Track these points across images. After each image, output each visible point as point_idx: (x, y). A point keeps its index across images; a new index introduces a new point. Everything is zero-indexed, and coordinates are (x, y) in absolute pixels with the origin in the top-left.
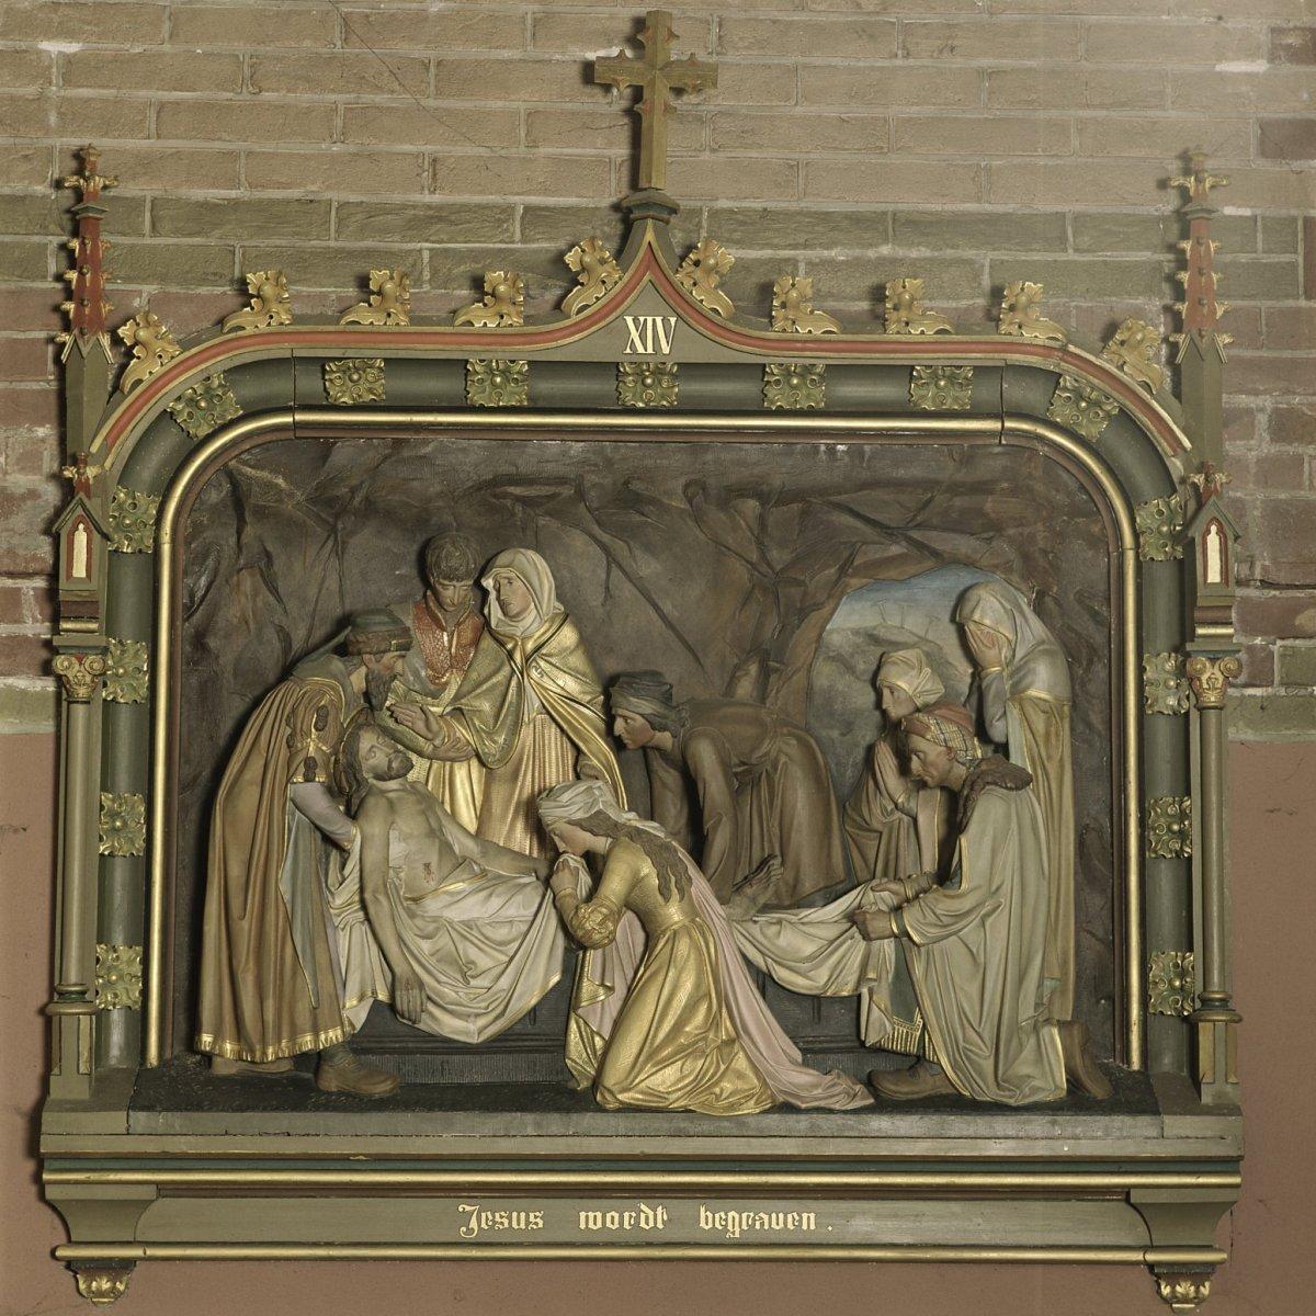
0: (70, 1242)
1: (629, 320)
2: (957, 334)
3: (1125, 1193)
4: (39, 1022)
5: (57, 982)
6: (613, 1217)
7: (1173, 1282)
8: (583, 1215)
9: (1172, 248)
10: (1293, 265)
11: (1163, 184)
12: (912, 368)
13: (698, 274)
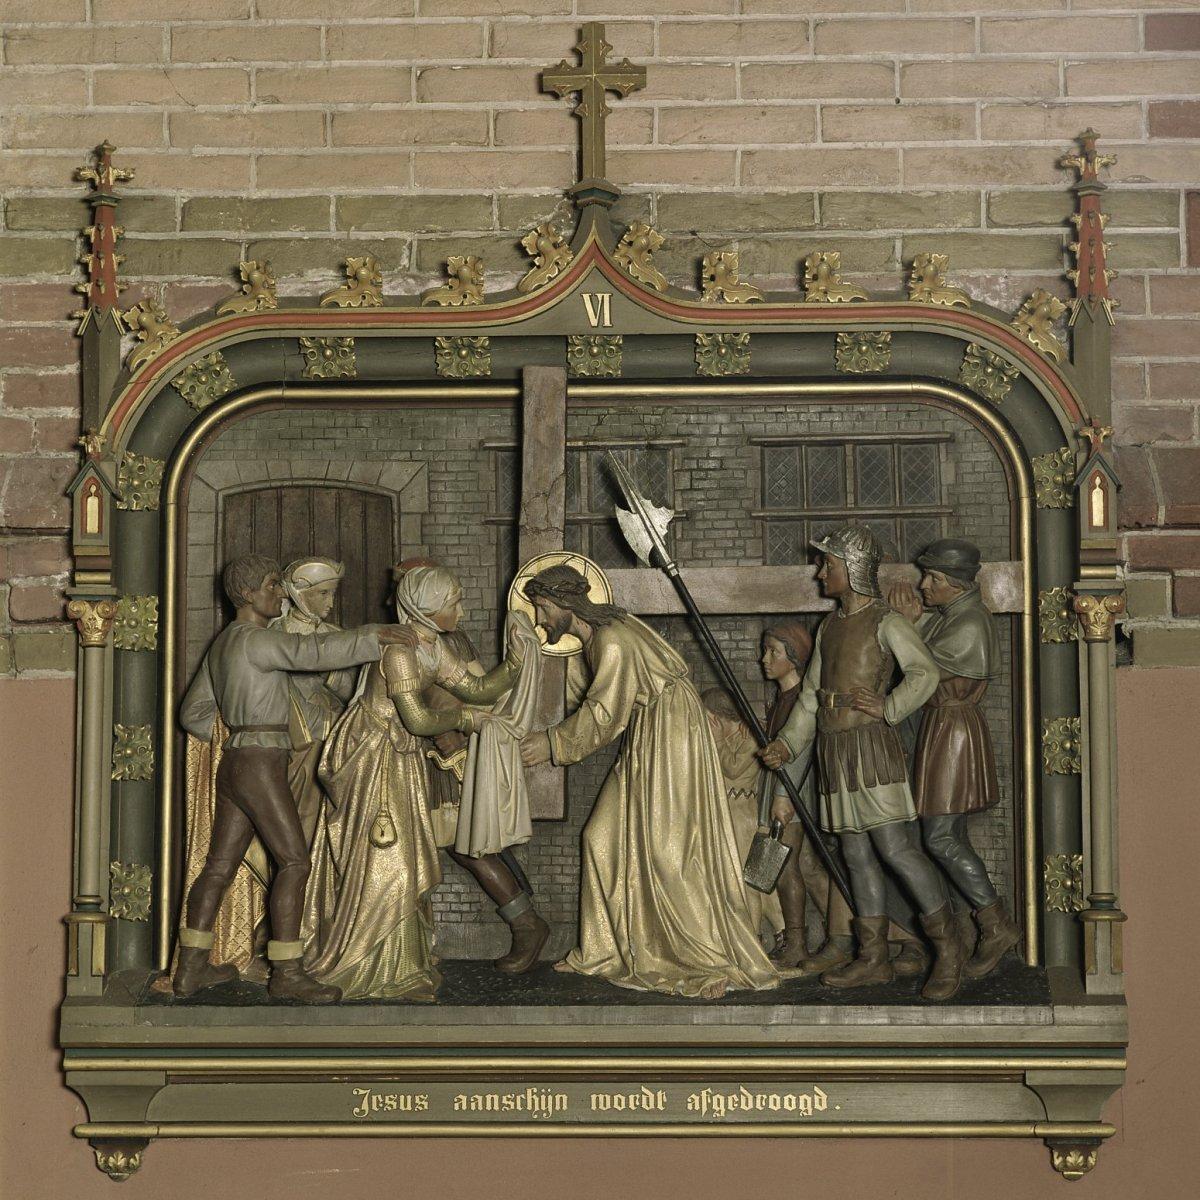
0: (89, 1122)
1: (586, 297)
2: (766, 302)
3: (1020, 1077)
4: (61, 929)
5: (75, 895)
6: (790, 1100)
7: (109, 1152)
8: (594, 1097)
9: (1067, 223)
10: (1176, 237)
11: (1059, 166)
12: (836, 334)
13: (632, 254)
